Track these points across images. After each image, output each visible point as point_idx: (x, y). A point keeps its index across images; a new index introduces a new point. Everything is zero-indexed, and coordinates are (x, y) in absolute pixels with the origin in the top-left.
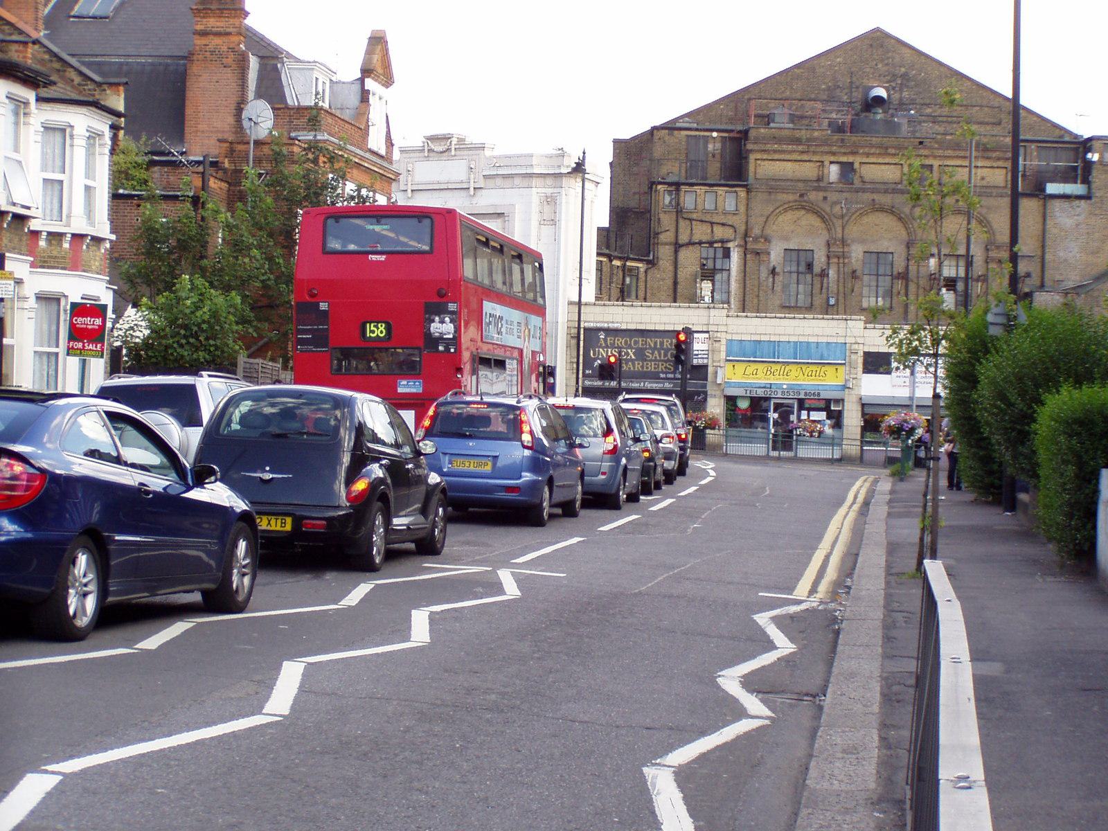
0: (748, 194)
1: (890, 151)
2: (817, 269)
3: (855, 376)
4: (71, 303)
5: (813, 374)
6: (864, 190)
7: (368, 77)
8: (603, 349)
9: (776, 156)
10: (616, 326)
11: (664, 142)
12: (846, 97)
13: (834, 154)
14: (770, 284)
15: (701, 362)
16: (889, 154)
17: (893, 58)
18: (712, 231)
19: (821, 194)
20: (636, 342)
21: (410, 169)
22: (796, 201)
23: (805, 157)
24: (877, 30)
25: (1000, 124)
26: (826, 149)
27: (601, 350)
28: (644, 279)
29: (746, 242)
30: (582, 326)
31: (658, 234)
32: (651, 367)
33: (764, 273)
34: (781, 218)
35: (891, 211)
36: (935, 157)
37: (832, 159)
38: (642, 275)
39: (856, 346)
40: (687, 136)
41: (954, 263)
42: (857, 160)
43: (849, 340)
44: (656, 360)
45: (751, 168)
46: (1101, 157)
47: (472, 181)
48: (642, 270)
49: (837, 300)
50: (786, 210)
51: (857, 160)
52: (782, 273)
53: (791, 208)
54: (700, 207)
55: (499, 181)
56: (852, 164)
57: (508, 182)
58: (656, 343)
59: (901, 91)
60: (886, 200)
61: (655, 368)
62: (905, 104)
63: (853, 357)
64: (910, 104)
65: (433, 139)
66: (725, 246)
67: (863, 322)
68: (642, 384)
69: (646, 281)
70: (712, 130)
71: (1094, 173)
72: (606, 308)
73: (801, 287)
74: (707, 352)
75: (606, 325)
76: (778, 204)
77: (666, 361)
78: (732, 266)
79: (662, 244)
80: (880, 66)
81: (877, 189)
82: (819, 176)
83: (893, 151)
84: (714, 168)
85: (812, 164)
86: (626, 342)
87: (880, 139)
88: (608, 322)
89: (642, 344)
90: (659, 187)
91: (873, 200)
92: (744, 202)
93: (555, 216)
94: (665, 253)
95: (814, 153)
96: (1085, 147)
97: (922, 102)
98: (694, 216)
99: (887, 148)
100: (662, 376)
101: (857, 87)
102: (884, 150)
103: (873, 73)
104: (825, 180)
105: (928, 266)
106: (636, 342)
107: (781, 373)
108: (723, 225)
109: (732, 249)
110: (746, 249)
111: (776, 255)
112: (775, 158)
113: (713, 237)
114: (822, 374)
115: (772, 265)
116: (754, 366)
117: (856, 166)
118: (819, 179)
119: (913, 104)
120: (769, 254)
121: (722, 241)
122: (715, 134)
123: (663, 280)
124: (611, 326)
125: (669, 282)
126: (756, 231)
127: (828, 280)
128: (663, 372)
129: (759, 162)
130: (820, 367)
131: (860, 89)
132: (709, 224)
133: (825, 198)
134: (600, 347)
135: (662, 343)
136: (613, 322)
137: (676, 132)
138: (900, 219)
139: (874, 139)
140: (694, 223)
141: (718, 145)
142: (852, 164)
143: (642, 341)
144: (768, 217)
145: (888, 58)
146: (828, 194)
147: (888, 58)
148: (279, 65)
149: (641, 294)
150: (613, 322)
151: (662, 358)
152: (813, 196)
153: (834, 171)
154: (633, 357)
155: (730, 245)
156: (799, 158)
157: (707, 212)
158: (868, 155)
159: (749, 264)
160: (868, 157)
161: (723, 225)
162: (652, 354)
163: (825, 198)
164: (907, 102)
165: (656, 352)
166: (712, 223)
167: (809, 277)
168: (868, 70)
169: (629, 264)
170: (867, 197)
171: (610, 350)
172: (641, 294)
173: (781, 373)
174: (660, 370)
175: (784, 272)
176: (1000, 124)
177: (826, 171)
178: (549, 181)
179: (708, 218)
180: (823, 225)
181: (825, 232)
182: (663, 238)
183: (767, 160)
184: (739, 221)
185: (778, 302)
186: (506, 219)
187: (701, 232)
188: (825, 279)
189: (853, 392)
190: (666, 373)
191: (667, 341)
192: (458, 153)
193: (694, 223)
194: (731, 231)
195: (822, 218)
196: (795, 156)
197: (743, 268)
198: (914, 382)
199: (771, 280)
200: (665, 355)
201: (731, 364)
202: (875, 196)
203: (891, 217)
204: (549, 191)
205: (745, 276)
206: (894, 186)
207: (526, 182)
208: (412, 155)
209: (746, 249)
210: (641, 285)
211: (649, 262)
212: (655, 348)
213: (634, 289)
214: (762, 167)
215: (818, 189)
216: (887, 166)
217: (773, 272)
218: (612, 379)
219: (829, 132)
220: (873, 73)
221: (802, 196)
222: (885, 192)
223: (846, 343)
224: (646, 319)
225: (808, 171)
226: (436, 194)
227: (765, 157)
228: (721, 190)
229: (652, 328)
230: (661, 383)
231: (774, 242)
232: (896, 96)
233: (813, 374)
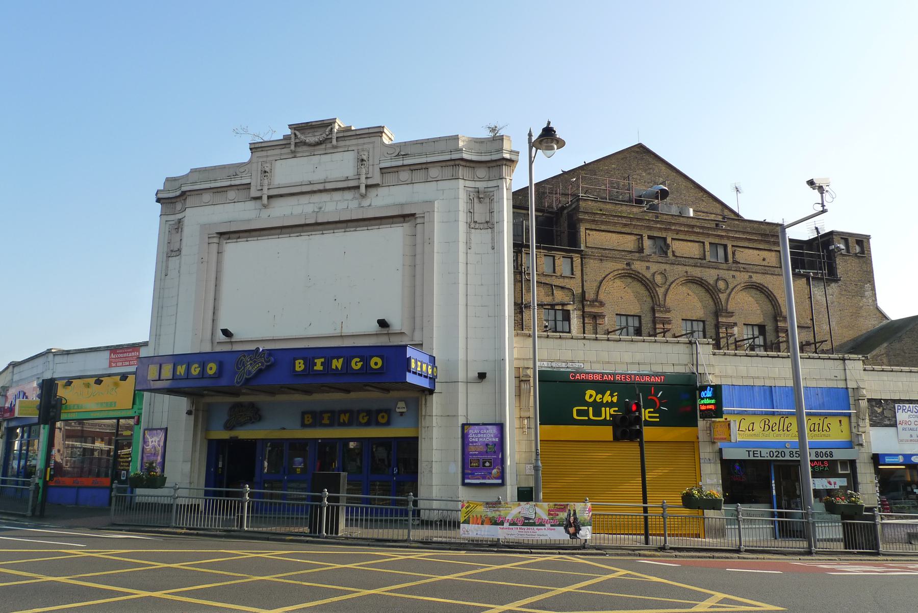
4: (205, 487)
5: (816, 428)
9: (603, 227)
17: (653, 169)
21: (267, 169)
22: (624, 269)
36: (728, 238)
47: (363, 177)
55: (404, 175)
56: (665, 239)
57: (420, 175)
65: (298, 128)
66: (565, 308)
72: (563, 341)
78: (572, 328)
107: (821, 428)
108: (562, 288)
109: (571, 312)
110: (584, 312)
114: (825, 428)
116: (749, 419)
117: (669, 241)
121: (563, 305)
126: (590, 295)
130: (822, 419)
132: (549, 286)
136: (572, 362)
144: (601, 282)
150: (572, 362)
158: (678, 232)
160: (677, 234)
173: (821, 428)
178: (481, 172)
180: (647, 293)
186: (419, 221)
189: (863, 450)
192: (341, 143)
202: (689, 269)
204: (481, 185)
207: (448, 172)
208: (270, 153)
214: (590, 238)
216: (692, 244)
226: (304, 199)
233: (816, 428)
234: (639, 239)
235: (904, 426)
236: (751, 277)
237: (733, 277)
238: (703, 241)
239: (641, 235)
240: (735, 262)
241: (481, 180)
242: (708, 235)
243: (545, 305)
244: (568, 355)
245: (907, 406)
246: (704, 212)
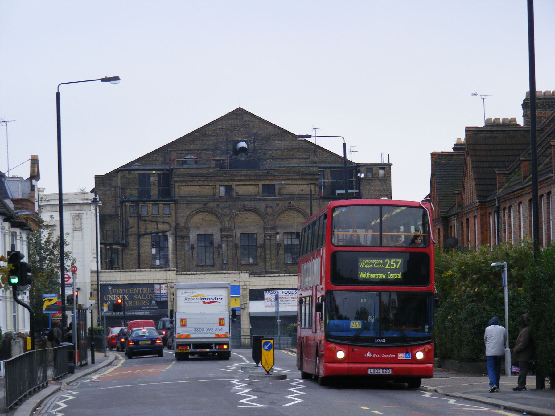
0: (175, 205)
1: (252, 178)
2: (216, 245)
3: (246, 302)
4: (280, 316)
6: (239, 200)
7: (34, 179)
8: (111, 295)
10: (117, 282)
11: (126, 177)
12: (224, 147)
13: (221, 181)
14: (191, 254)
15: (164, 299)
16: (251, 180)
17: (249, 125)
18: (157, 226)
19: (216, 203)
20: (129, 291)
22: (202, 208)
23: (206, 183)
24: (240, 109)
25: (309, 158)
26: (217, 178)
27: (110, 296)
28: (121, 254)
29: (176, 231)
30: (99, 283)
31: (128, 229)
32: (137, 304)
33: (187, 248)
34: (194, 217)
35: (254, 210)
36: (276, 180)
37: (221, 183)
38: (120, 253)
39: (245, 287)
40: (139, 173)
41: (290, 237)
42: (234, 184)
43: (241, 284)
44: (139, 299)
45: (177, 190)
46: (365, 175)
48: (120, 250)
49: (228, 261)
50: (197, 213)
51: (234, 184)
52: (196, 247)
53: (200, 212)
54: (150, 213)
56: (231, 185)
58: (139, 291)
59: (254, 142)
60: (251, 204)
61: (139, 304)
62: (256, 150)
63: (245, 292)
64: (259, 150)
66: (165, 234)
67: (248, 274)
68: (133, 313)
69: (122, 256)
70: (153, 170)
71: (362, 184)
72: (112, 274)
73: (207, 255)
74: (166, 294)
75: (112, 283)
76: (193, 209)
77: (145, 300)
78: (169, 245)
79: (130, 235)
80: (242, 129)
81: (245, 199)
82: (214, 193)
83: (253, 178)
84: (155, 192)
85: (210, 187)
86: (123, 291)
87: (246, 171)
88: (113, 281)
89: (132, 292)
90: (127, 204)
91: (244, 205)
92: (174, 209)
93: (81, 226)
94: (132, 240)
95: (211, 181)
96: (356, 170)
97: (266, 148)
98: (147, 219)
99: (250, 176)
100: (143, 308)
101: (230, 142)
102: (248, 178)
103: (238, 134)
104: (217, 195)
105: (276, 240)
106: (129, 291)
108: (163, 222)
109: (168, 236)
110: (176, 235)
111: (193, 237)
112: (189, 185)
113: (158, 230)
115: (191, 243)
117: (234, 186)
118: (214, 195)
119: (261, 149)
120: (189, 237)
122: (154, 172)
123: (132, 254)
124: (115, 283)
125: (135, 256)
126: (182, 225)
127: (222, 250)
128: (144, 306)
129: (180, 187)
131: (232, 143)
132: (155, 224)
133: (218, 205)
134: (110, 294)
135: (142, 291)
137: (132, 172)
138: (259, 215)
139: (243, 172)
140: (147, 222)
141: (156, 178)
142: (231, 185)
143: (132, 290)
145: (246, 125)
146: (220, 203)
147: (246, 125)
148: (3, 179)
149: (120, 264)
151: (143, 298)
152: (212, 205)
153: (222, 190)
154: (127, 299)
155: (168, 233)
156: (202, 184)
157: (153, 216)
158: (240, 181)
159: (178, 243)
161: (163, 222)
162: (138, 296)
163: (218, 205)
164: (258, 149)
165: (139, 295)
166: (157, 222)
167: (211, 249)
168: (235, 132)
169: (114, 247)
170: (240, 204)
171: (114, 296)
172: (120, 264)
174: (142, 305)
175: (198, 247)
176: (309, 158)
177: (217, 190)
179: (155, 219)
181: (219, 224)
182: (130, 231)
183: (185, 186)
184: (171, 220)
185: (195, 264)
187: (151, 228)
188: (221, 249)
189: (245, 311)
190: (146, 306)
191: (145, 289)
193: (147, 222)
194: (168, 225)
195: (216, 216)
196: (200, 183)
197: (175, 246)
198: (278, 304)
199: (191, 251)
200: (145, 297)
201: (234, 299)
202: (245, 203)
203: (254, 214)
204: (77, 212)
205: (176, 250)
206: (254, 197)
209: (176, 235)
210: (120, 257)
211: (123, 245)
212: (139, 293)
213: (116, 260)
215: (214, 200)
216: (250, 186)
217: (192, 247)
218: (120, 311)
219: (218, 169)
220: (238, 134)
221: (205, 205)
222: (250, 201)
223: (240, 285)
224: (133, 278)
225: (207, 190)
227: (184, 184)
228: (161, 204)
229: (135, 282)
230: (143, 312)
231: (191, 231)
232: (252, 145)
234: (214, 188)
235: (268, 300)
236: (290, 203)
237: (278, 204)
238: (258, 184)
239: (215, 185)
240: (280, 195)
241: (78, 210)
242: (261, 180)
243: (153, 233)
244: (128, 278)
245: (271, 291)
246: (287, 149)
